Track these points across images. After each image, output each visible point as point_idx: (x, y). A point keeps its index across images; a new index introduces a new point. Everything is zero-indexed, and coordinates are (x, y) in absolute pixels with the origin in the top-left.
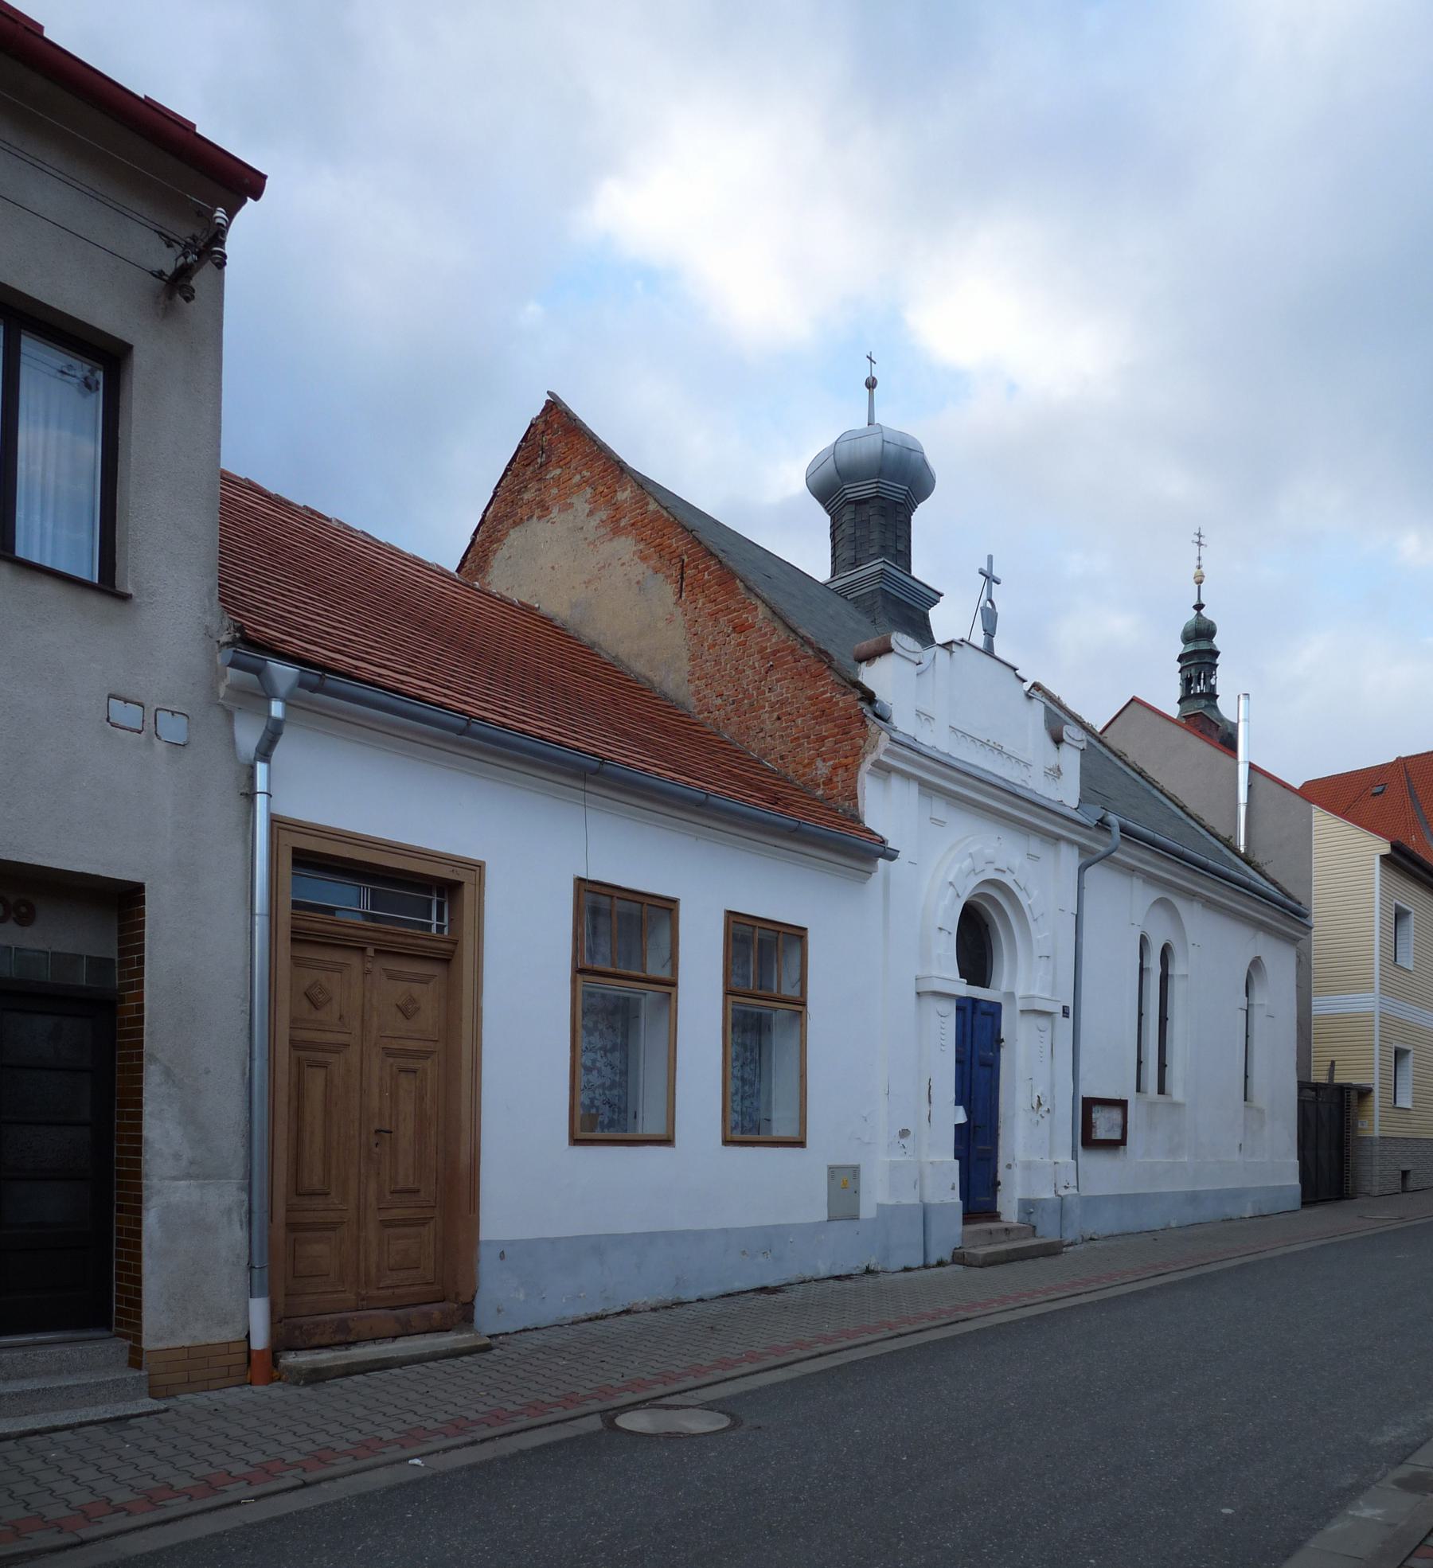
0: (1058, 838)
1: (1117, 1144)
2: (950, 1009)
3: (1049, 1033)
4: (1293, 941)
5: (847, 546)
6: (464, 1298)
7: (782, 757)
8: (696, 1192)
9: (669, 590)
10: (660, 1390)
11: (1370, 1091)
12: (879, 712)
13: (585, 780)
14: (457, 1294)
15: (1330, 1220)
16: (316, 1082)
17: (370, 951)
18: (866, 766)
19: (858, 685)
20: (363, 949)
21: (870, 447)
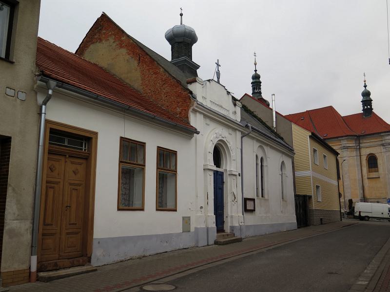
0: (236, 129)
1: (253, 211)
2: (212, 173)
6: (89, 256)
8: (149, 224)
9: (136, 63)
10: (150, 280)
11: (311, 197)
12: (194, 96)
13: (124, 112)
15: (305, 232)
17: (67, 156)
18: (191, 110)
19: (189, 90)
21: (182, 29)
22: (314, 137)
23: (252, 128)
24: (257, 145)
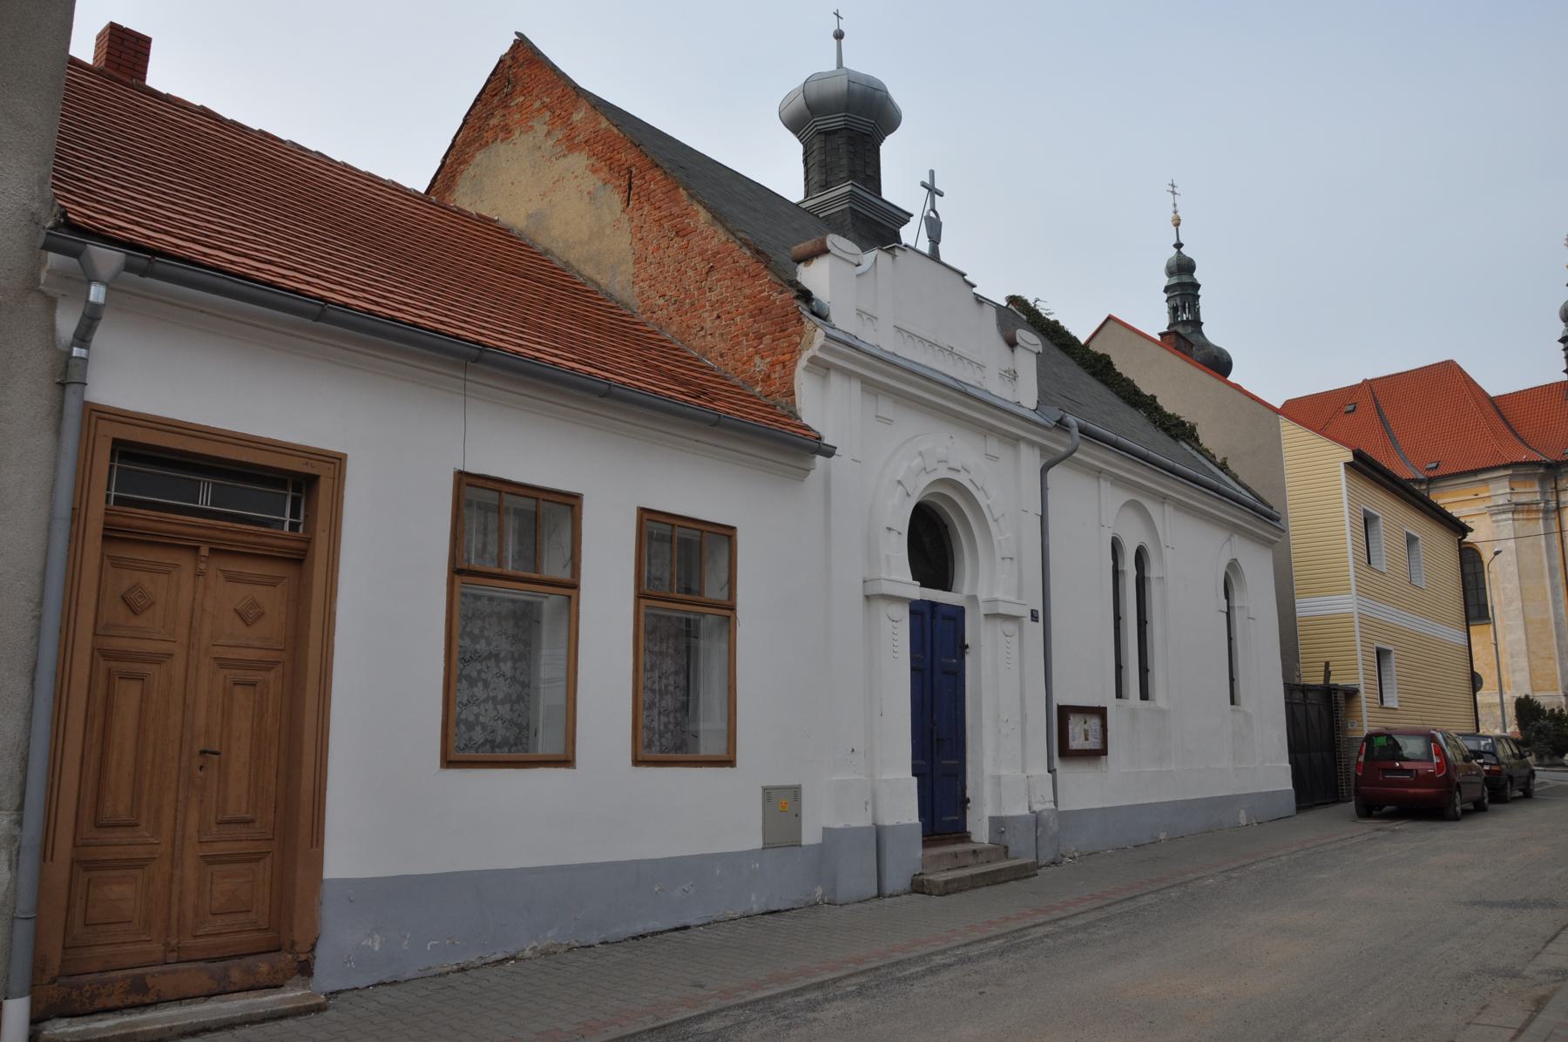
0: (1018, 439)
1: (1098, 753)
3: (1015, 639)
4: (1268, 543)
5: (818, 171)
7: (722, 355)
8: (599, 810)
9: (617, 200)
14: (293, 944)
16: (128, 697)
17: (204, 551)
18: (803, 362)
19: (795, 284)
20: (197, 549)
22: (1364, 467)
23: (1083, 431)
24: (1113, 498)
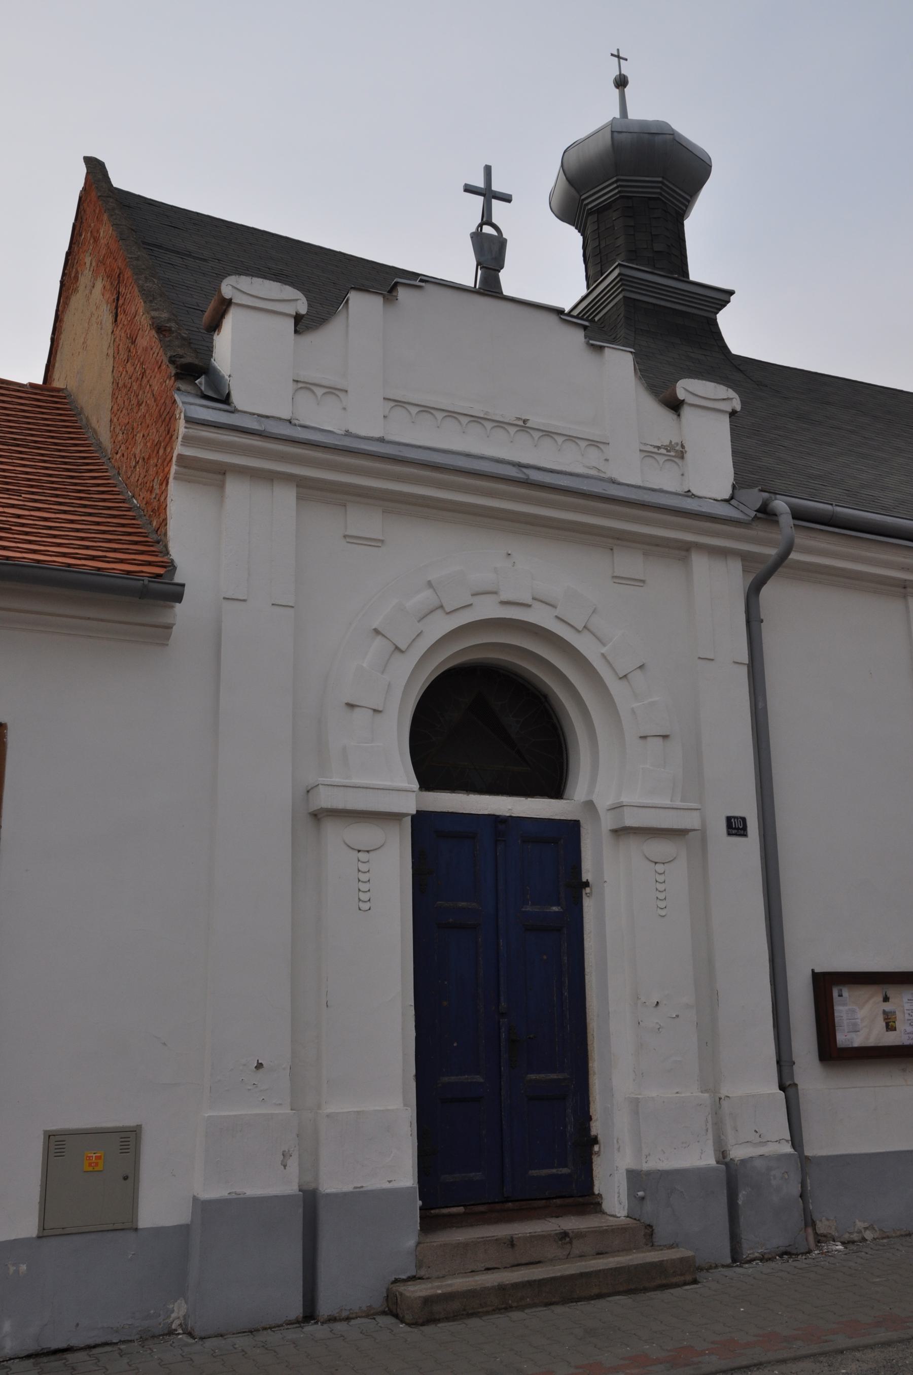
0: (686, 549)
